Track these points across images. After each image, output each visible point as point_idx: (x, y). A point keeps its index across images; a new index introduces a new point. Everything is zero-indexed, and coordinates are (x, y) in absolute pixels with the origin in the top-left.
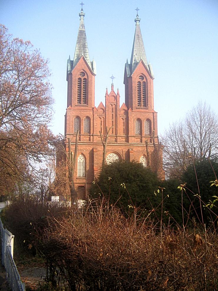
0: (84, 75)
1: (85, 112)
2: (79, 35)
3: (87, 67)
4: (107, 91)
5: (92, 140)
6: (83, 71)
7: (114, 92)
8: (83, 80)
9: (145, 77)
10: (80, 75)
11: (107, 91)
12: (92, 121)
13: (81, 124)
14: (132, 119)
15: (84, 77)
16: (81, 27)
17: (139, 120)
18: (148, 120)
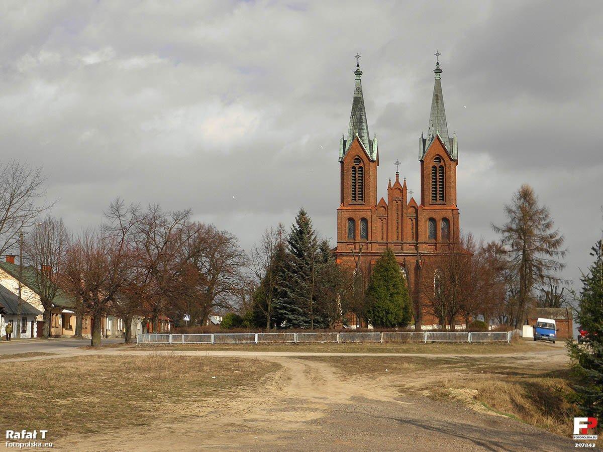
0: (360, 162)
1: (361, 213)
2: (354, 104)
3: (363, 152)
4: (390, 183)
5: (370, 249)
6: (357, 157)
7: (399, 183)
8: (357, 170)
9: (362, 160)
10: (354, 162)
11: (390, 183)
12: (369, 224)
13: (356, 228)
14: (423, 219)
15: (360, 165)
16: (357, 93)
17: (432, 220)
18: (445, 220)
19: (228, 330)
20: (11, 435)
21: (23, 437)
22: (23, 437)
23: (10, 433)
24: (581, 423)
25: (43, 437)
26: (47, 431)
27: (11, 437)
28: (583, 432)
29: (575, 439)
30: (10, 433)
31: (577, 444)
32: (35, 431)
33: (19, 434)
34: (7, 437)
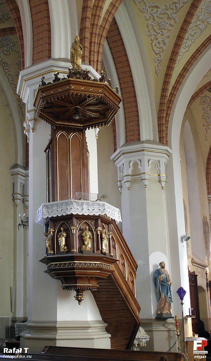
19: (67, 170)
20: (7, 351)
21: (14, 352)
22: (14, 352)
23: (6, 350)
24: (198, 344)
25: (26, 352)
26: (28, 349)
27: (7, 352)
28: (199, 349)
29: (194, 353)
30: (6, 350)
31: (195, 356)
32: (21, 349)
33: (11, 350)
34: (4, 352)
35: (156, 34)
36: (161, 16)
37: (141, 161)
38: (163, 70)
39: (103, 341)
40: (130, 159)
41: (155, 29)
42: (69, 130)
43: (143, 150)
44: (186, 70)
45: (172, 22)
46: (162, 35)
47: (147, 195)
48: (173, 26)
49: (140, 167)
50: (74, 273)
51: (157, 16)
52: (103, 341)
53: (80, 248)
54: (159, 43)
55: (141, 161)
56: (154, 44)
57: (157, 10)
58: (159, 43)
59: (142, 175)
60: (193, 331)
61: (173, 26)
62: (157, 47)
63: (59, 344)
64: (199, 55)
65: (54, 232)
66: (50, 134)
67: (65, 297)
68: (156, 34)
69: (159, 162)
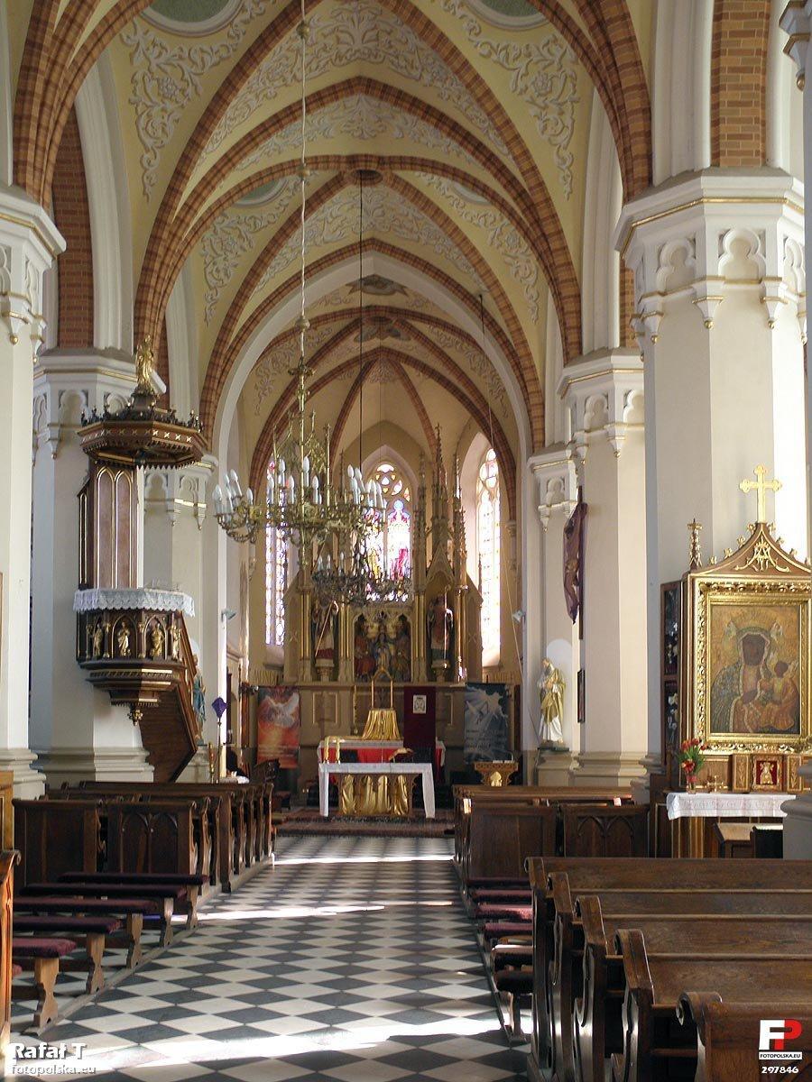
35: (149, 104)
36: (229, 230)
37: (87, 395)
38: (158, 195)
39: (146, 775)
40: (61, 387)
41: (215, 247)
42: (116, 467)
43: (95, 371)
44: (254, 320)
45: (245, 244)
46: (225, 259)
47: (174, 540)
48: (245, 250)
49: (164, 487)
50: (140, 685)
51: (157, 65)
52: (146, 775)
53: (148, 652)
54: (218, 271)
55: (87, 395)
56: (208, 270)
57: (223, 221)
58: (218, 271)
59: (168, 503)
60: (227, 767)
61: (245, 250)
62: (148, 133)
63: (99, 778)
64: (280, 300)
65: (110, 629)
66: (88, 468)
67: (104, 713)
68: (215, 256)
69: (198, 480)
